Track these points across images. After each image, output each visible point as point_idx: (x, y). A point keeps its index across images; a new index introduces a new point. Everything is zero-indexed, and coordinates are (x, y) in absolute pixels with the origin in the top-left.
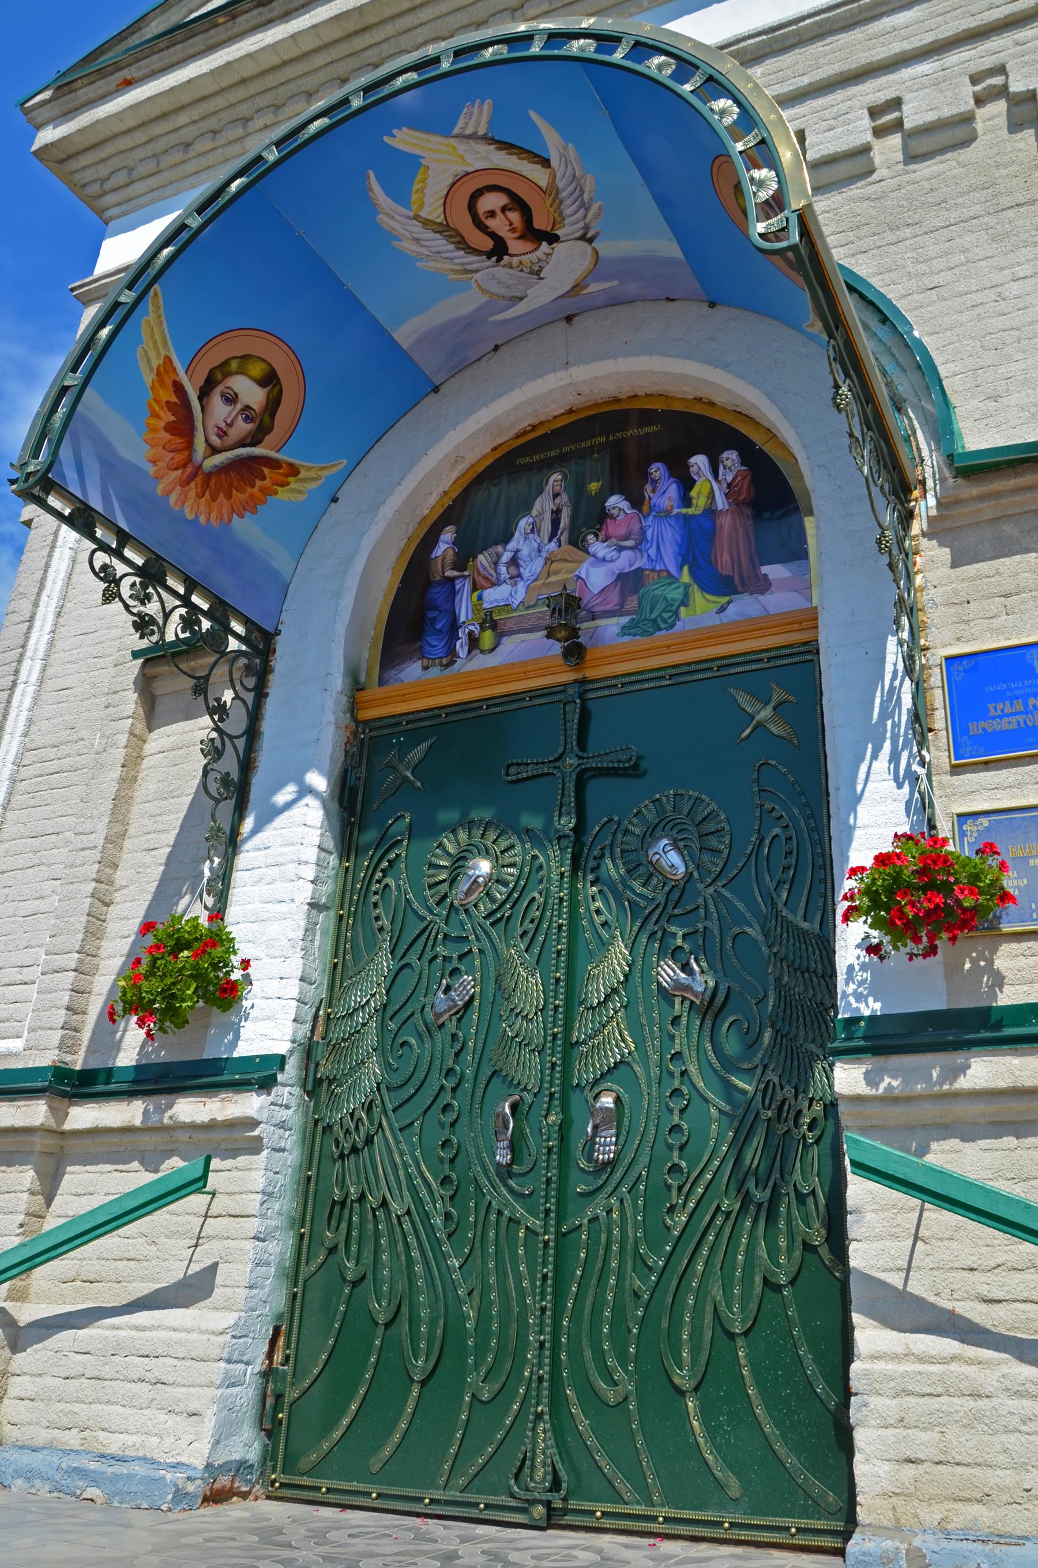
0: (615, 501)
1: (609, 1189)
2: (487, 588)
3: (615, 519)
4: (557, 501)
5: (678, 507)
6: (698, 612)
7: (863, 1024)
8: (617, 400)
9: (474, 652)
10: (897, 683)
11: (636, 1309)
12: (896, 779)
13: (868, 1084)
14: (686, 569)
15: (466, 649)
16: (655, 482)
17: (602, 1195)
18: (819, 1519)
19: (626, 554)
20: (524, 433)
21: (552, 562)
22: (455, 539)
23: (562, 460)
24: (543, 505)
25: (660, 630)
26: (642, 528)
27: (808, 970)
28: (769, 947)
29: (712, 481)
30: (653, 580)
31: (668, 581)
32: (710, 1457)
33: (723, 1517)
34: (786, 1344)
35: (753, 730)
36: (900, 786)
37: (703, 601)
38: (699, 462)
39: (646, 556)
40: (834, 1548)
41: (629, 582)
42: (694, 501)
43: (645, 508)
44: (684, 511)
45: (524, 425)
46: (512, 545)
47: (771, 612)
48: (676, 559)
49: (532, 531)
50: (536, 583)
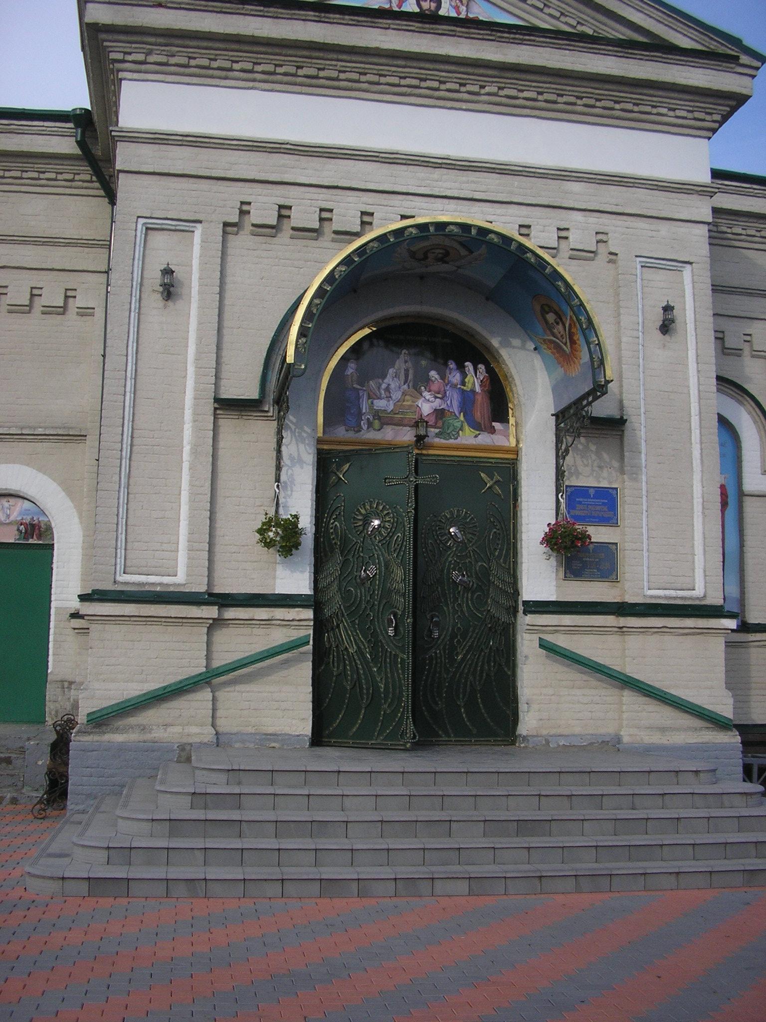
0: (433, 374)
16: (451, 369)
41: (439, 414)
46: (386, 381)
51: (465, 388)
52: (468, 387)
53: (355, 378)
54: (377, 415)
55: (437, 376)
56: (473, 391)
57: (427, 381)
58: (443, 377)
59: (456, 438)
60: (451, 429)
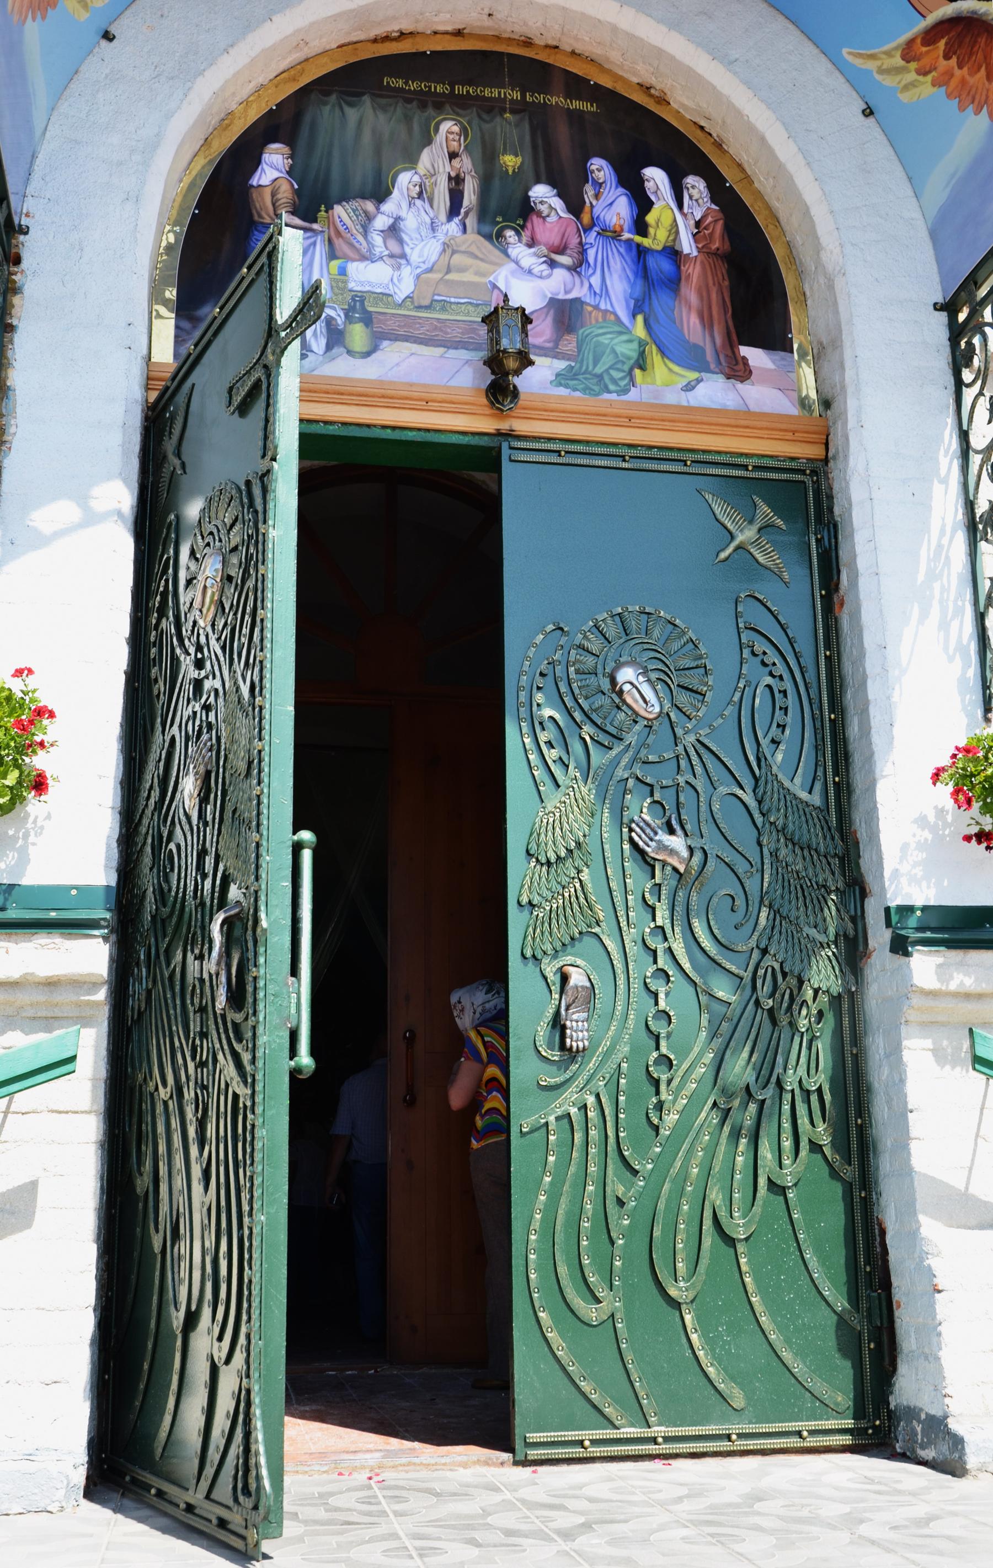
0: (541, 192)
1: (581, 1081)
2: (354, 260)
3: (544, 218)
4: (456, 162)
5: (629, 232)
6: (659, 382)
7: (918, 913)
8: (528, 43)
9: (336, 350)
10: (945, 541)
11: (620, 1218)
12: (946, 649)
13: (939, 980)
14: (640, 318)
15: (323, 342)
16: (598, 185)
17: (573, 1088)
18: (827, 1420)
19: (560, 273)
20: (387, 38)
21: (454, 252)
22: (291, 167)
23: (458, 104)
24: (433, 160)
25: (609, 392)
26: (581, 243)
27: (809, 847)
28: (764, 815)
29: (679, 216)
30: (597, 321)
31: (617, 329)
32: (711, 1369)
33: (729, 1429)
34: (789, 1247)
35: (735, 550)
36: (951, 659)
37: (665, 370)
38: (656, 177)
39: (586, 285)
40: (843, 1446)
41: (566, 314)
42: (651, 231)
43: (586, 218)
44: (638, 239)
45: (394, 27)
46: (388, 207)
47: (752, 410)
48: (627, 301)
49: (420, 195)
50: (429, 275)
51: (646, 242)
52: (657, 239)
53: (285, 192)
54: (359, 308)
55: (557, 203)
56: (673, 253)
57: (524, 212)
58: (575, 206)
59: (625, 391)
60: (607, 361)
